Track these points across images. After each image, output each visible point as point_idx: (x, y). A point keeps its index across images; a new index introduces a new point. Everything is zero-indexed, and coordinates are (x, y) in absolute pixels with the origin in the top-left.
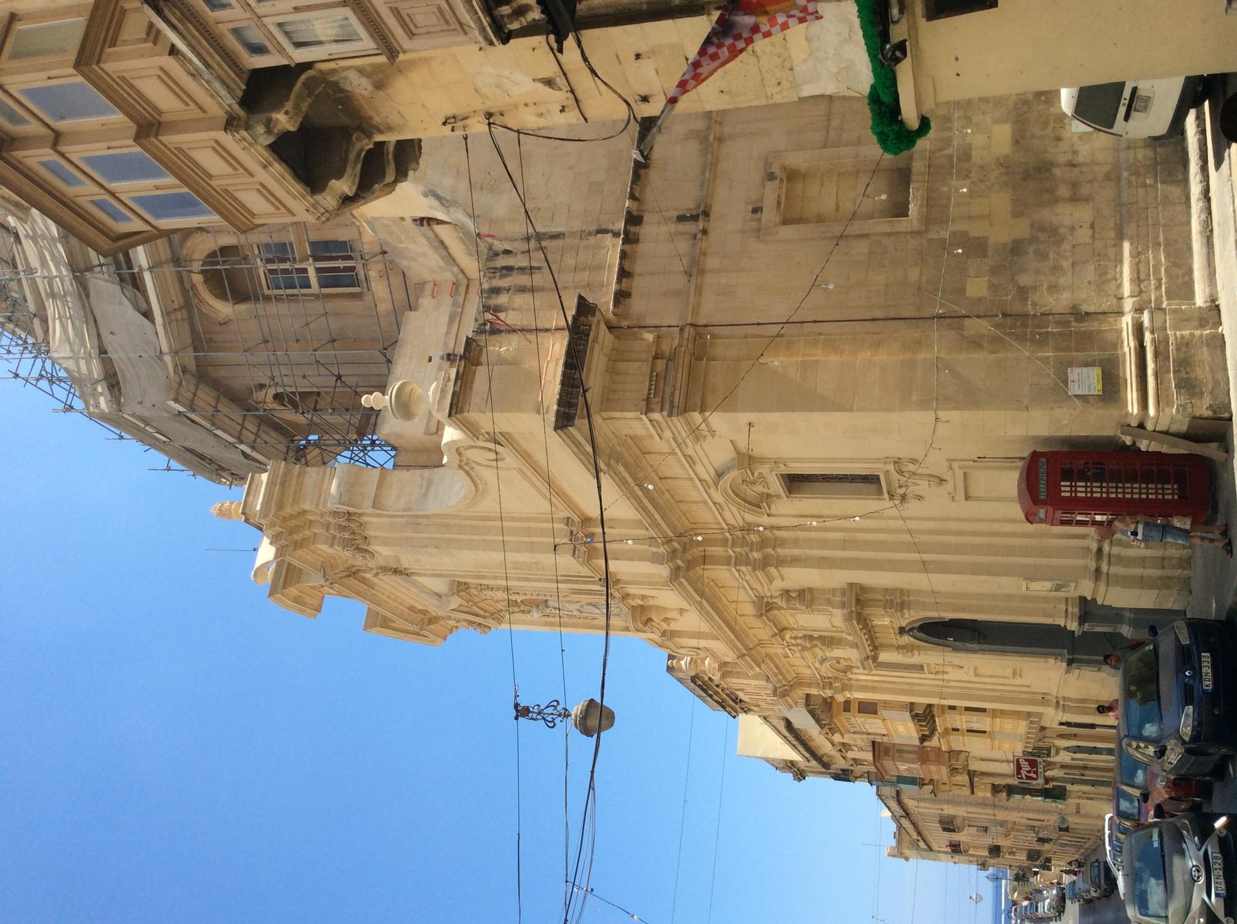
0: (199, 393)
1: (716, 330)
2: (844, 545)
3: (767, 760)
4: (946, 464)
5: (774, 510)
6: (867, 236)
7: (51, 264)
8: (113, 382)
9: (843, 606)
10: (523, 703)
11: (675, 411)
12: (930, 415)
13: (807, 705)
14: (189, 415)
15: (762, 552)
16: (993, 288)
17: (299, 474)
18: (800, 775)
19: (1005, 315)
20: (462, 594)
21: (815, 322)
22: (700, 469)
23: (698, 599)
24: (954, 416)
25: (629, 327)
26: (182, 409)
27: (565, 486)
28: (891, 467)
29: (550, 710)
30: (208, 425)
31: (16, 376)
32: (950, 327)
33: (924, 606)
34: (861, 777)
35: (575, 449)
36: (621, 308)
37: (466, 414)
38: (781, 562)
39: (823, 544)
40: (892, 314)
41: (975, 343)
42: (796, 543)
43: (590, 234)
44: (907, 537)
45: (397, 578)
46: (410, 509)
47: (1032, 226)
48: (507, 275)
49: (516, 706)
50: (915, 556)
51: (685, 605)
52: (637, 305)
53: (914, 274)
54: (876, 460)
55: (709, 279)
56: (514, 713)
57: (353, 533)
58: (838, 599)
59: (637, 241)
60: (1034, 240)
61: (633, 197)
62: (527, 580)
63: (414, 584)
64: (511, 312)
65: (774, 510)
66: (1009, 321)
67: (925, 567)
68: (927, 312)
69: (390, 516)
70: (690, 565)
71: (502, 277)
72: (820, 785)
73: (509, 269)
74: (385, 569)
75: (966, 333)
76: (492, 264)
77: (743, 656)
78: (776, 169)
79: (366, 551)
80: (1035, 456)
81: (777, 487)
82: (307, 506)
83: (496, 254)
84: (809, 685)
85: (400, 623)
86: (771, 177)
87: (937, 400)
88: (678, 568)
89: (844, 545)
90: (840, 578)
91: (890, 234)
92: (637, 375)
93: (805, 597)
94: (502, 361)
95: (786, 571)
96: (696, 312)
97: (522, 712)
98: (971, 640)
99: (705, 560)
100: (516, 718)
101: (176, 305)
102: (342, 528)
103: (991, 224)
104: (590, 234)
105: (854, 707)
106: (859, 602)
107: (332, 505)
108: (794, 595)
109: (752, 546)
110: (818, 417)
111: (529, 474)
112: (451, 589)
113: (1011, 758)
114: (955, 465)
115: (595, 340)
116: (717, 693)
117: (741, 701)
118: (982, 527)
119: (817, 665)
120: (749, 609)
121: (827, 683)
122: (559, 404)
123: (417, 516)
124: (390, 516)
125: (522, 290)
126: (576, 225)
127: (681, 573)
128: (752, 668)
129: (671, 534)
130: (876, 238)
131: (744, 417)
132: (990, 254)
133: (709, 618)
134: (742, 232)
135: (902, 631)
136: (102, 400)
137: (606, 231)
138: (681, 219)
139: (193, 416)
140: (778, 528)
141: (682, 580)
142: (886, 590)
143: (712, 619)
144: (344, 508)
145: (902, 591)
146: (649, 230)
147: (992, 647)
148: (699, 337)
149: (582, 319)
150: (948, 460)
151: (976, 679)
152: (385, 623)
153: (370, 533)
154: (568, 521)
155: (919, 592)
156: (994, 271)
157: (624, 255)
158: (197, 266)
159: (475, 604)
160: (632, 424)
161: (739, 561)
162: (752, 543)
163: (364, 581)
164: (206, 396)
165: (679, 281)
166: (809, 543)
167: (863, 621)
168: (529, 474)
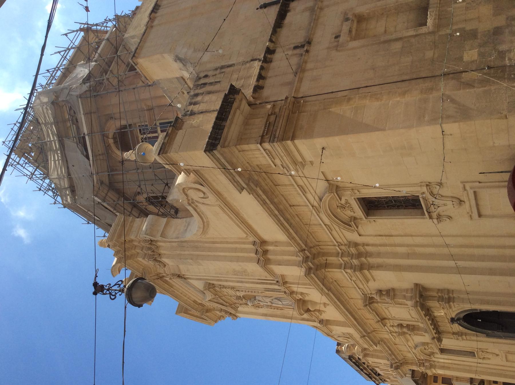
0: (109, 194)
1: (307, 99)
2: (408, 256)
4: (461, 186)
5: (361, 230)
6: (401, 39)
7: (51, 135)
8: (73, 190)
9: (411, 298)
10: (100, 282)
11: (276, 140)
12: (437, 129)
13: (413, 377)
14: (102, 203)
15: (360, 260)
16: (481, 54)
17: (131, 222)
19: (489, 68)
20: (211, 290)
21: (367, 87)
22: (309, 196)
23: (327, 292)
24: (452, 128)
25: (260, 104)
26: (99, 201)
27: (245, 216)
28: (424, 189)
29: (116, 288)
30: (112, 210)
31: (40, 189)
32: (453, 78)
33: (463, 301)
35: (269, 213)
36: (257, 95)
37: (168, 154)
38: (370, 267)
39: (395, 255)
40: (415, 76)
41: (469, 85)
42: (379, 255)
43: (247, 62)
44: (445, 251)
46: (178, 238)
47: (507, 19)
48: (203, 87)
49: (95, 284)
50: (452, 263)
52: (266, 93)
53: (429, 54)
55: (307, 74)
56: (93, 290)
57: (153, 251)
58: (409, 295)
59: (271, 61)
60: (508, 26)
61: (271, 40)
62: (242, 282)
63: (189, 284)
64: (202, 104)
65: (362, 232)
66: (492, 71)
67: (459, 271)
68: (438, 73)
69: (170, 242)
70: (318, 267)
71: (201, 88)
73: (205, 84)
74: (173, 275)
75: (462, 80)
76: (197, 83)
77: (364, 336)
78: (350, 16)
79: (160, 262)
81: (359, 212)
82: (132, 237)
83: (200, 78)
84: (412, 364)
85: (193, 312)
86: (347, 19)
87: (442, 118)
88: (310, 268)
89: (408, 256)
91: (416, 36)
92: (258, 125)
93: (390, 293)
94: (192, 126)
95: (376, 273)
96: (297, 90)
97: (98, 289)
99: (327, 265)
100: (95, 293)
101: (100, 153)
102: (150, 249)
103: (479, 22)
104: (247, 62)
105: (440, 380)
106: (422, 296)
107: (143, 236)
108: (384, 293)
109: (352, 256)
110: (364, 137)
111: (234, 219)
112: (205, 287)
115: (238, 108)
116: (365, 369)
117: (379, 375)
118: (492, 241)
119: (413, 350)
120: (360, 303)
121: (421, 363)
122: (209, 139)
123: (182, 242)
124: (170, 242)
125: (209, 93)
126: (241, 59)
127: (312, 271)
128: (371, 346)
129: (304, 247)
130: (406, 40)
131: (319, 142)
132: (479, 37)
133: (342, 313)
134: (328, 48)
135: (453, 320)
136: (68, 197)
137: (256, 60)
138: (296, 48)
139: (105, 204)
140: (368, 245)
141: (313, 275)
142: (439, 290)
143: (340, 309)
144: (148, 237)
145: (448, 291)
146: (279, 55)
147: (511, 335)
148: (296, 104)
149: (231, 96)
150: (462, 182)
151: (509, 364)
152: (186, 312)
153: (162, 252)
154: (254, 243)
155: (460, 291)
156: (480, 46)
157: (262, 68)
158: (111, 136)
159: (220, 297)
160: (257, 154)
161: (346, 266)
162: (353, 255)
163: (166, 282)
164: (112, 195)
165: (290, 77)
166: (387, 255)
167: (428, 312)
168: (234, 219)
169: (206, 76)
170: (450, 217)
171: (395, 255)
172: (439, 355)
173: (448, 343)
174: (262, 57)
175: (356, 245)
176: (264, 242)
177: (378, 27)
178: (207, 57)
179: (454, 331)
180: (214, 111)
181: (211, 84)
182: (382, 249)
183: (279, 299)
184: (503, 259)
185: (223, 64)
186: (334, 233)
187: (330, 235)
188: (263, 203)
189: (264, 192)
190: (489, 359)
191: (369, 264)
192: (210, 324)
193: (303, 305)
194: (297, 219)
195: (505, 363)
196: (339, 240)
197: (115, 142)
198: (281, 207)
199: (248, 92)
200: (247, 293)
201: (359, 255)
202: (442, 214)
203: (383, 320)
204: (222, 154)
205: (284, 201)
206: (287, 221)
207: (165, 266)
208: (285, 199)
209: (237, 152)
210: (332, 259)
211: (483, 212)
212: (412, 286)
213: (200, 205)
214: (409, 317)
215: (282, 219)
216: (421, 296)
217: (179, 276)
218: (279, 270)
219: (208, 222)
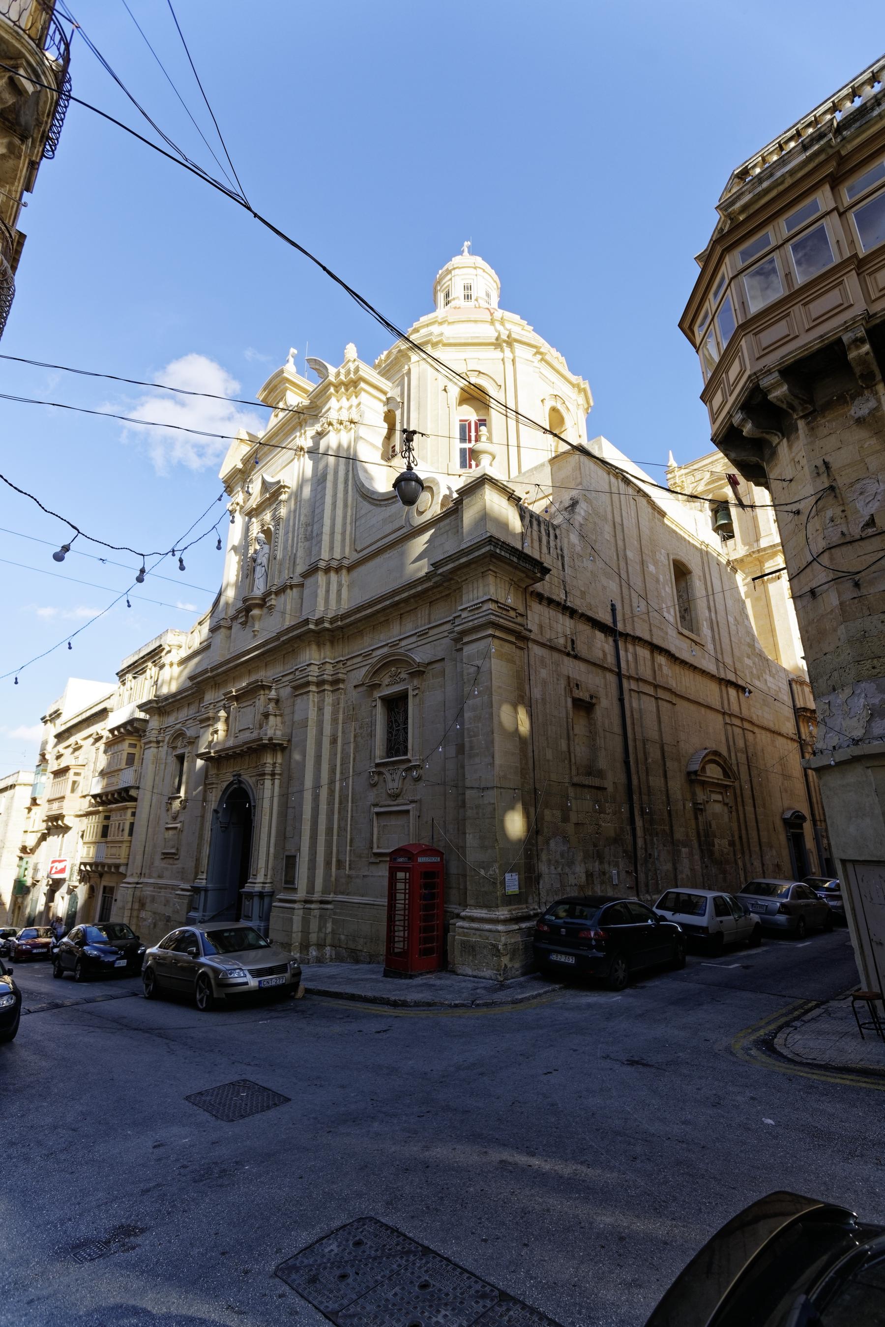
4: (417, 798)
40: (536, 763)
73: (548, 535)
83: (554, 530)
86: (591, 697)
138: (573, 641)
169: (556, 537)
174: (569, 604)
177: (580, 728)
178: (574, 538)
180: (652, 635)
181: (548, 542)
185: (566, 559)
194: (383, 619)
198: (402, 605)
199: (538, 587)
205: (408, 609)
215: (388, 603)
219: (381, 506)
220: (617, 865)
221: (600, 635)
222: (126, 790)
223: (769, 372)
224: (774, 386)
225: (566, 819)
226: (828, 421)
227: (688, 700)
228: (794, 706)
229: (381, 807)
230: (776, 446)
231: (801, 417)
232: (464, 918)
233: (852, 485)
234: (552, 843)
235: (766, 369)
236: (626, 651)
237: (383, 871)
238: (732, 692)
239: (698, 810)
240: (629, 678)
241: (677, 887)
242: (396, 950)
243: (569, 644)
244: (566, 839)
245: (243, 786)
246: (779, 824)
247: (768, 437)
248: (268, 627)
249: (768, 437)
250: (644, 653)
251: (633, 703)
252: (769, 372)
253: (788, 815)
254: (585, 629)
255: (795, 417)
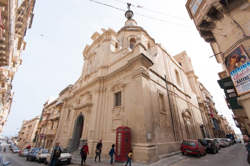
2: (102, 103)
3: (48, 100)
4: (123, 116)
18: (44, 105)
27: (116, 64)
34: (43, 113)
39: (102, 99)
42: (103, 96)
45: (98, 46)
49: (130, 4)
51: (88, 82)
54: (124, 105)
56: (129, 3)
72: (43, 107)
80: (129, 129)
81: (116, 91)
88: (100, 78)
90: (61, 117)
98: (77, 124)
99: (100, 83)
100: (128, 4)
106: (90, 105)
113: (44, 133)
114: (123, 117)
117: (62, 95)
143: (86, 85)
145: (90, 112)
153: (107, 42)
158: (134, 37)
163: (97, 42)
167: (85, 106)
169: (154, 59)
170: (113, 113)
171: (102, 99)
172: (68, 109)
173: (73, 112)
175: (106, 90)
176: (108, 68)
179: (77, 113)
182: (104, 97)
183: (90, 70)
184: (100, 125)
186: (110, 85)
187: (109, 85)
188: (122, 67)
189: (126, 68)
190: (66, 122)
191: (100, 93)
192: (83, 53)
193: (88, 76)
195: (64, 125)
196: (107, 86)
197: (132, 38)
198: (120, 72)
200: (92, 62)
201: (103, 91)
202: (114, 111)
203: (82, 96)
204: (140, 57)
206: (115, 73)
207: (103, 42)
208: (122, 73)
209: (140, 62)
210: (102, 84)
211: (114, 121)
212: (93, 103)
213: (121, 52)
214: (82, 102)
215: (117, 72)
216: (90, 105)
217: (99, 46)
218: (100, 71)
220: (171, 134)
221: (163, 81)
222: (57, 118)
223: (216, 2)
224: (218, 6)
225: (159, 121)
226: (233, 12)
227: (180, 98)
228: (198, 102)
229: (114, 118)
230: (216, 24)
231: (225, 13)
232: (136, 146)
233: (244, 24)
234: (157, 127)
235: (215, 2)
236: (168, 85)
237: (115, 134)
238: (188, 97)
239: (185, 122)
240: (169, 91)
241: (190, 139)
242: (118, 155)
243: (158, 81)
244: (160, 126)
245: (82, 115)
246: (199, 127)
247: (213, 21)
248: (90, 80)
249: (213, 21)
250: (172, 86)
251: (171, 96)
252: (216, 2)
253: (201, 125)
254: (160, 79)
255: (223, 13)
